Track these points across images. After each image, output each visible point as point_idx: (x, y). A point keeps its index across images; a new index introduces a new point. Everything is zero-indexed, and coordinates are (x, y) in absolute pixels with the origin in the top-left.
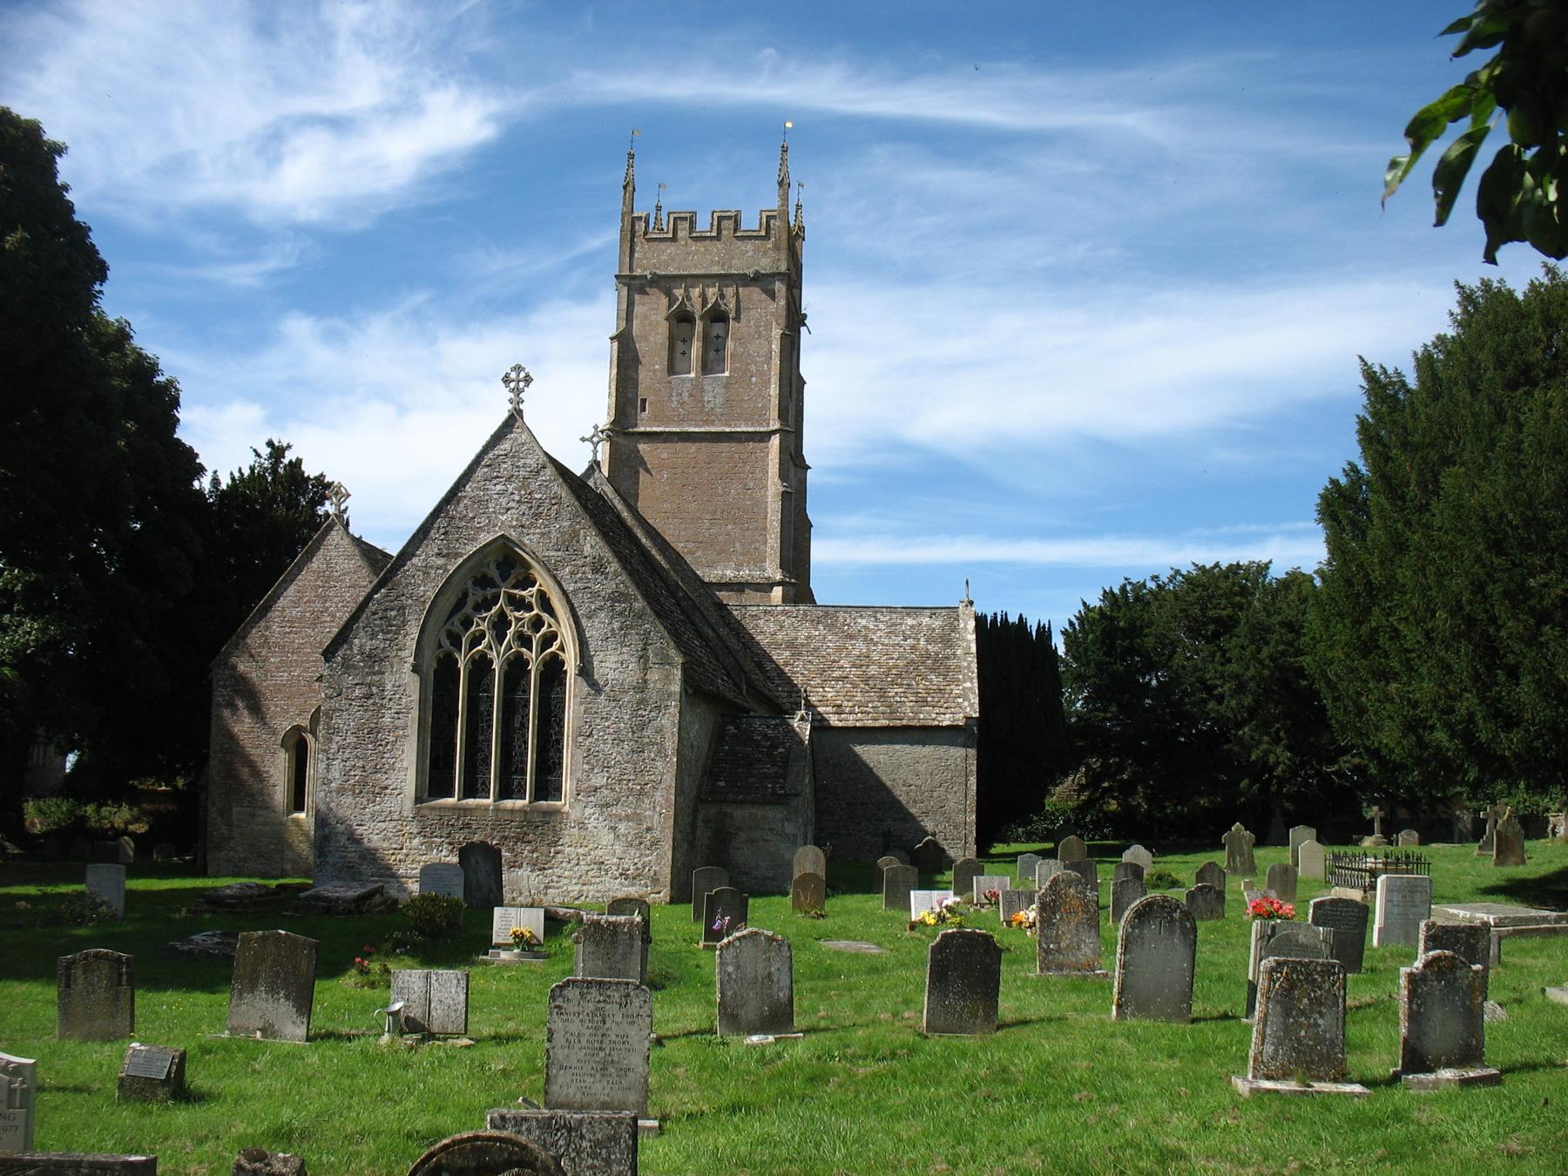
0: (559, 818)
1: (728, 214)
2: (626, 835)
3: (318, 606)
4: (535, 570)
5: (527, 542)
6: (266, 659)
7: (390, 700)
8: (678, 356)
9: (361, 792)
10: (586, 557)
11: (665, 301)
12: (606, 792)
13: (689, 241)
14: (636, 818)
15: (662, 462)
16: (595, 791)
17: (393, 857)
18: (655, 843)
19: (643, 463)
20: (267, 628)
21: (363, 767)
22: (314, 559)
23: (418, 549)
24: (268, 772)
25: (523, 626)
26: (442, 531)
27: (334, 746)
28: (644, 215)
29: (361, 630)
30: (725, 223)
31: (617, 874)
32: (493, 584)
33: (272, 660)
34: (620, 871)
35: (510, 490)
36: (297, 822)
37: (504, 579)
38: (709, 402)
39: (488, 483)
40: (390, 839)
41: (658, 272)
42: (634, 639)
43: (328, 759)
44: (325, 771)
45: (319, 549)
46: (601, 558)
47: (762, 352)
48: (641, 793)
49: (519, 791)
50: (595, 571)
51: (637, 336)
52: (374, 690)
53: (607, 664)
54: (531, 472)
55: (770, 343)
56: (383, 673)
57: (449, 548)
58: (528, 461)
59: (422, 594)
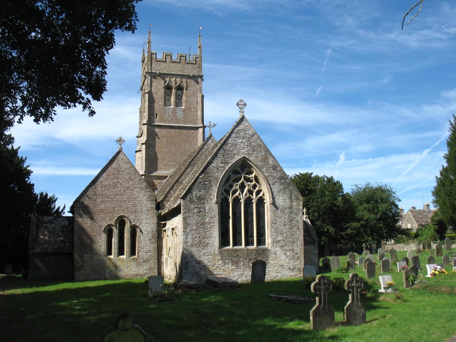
0: (268, 251)
1: (183, 55)
2: (289, 256)
3: (115, 181)
4: (254, 168)
5: (251, 159)
6: (96, 200)
7: (208, 213)
8: (166, 100)
9: (199, 246)
10: (270, 165)
11: (163, 82)
12: (282, 242)
13: (170, 63)
14: (292, 250)
15: (164, 135)
16: (279, 242)
17: (212, 268)
18: (298, 258)
19: (157, 135)
20: (96, 188)
21: (200, 237)
22: (113, 164)
23: (214, 160)
24: (98, 241)
25: (250, 187)
26: (222, 154)
27: (188, 230)
28: (155, 52)
29: (196, 189)
30: (168, 57)
31: (287, 269)
32: (239, 173)
33: (98, 200)
34: (288, 268)
35: (244, 142)
36: (110, 259)
37: (242, 172)
38: (178, 116)
39: (236, 139)
40: (211, 262)
41: (161, 72)
42: (287, 192)
43: (186, 234)
44: (185, 239)
45: (115, 160)
46: (275, 165)
47: (195, 101)
48: (293, 242)
49: (252, 243)
50: (274, 169)
51: (154, 93)
52: (202, 210)
53: (280, 200)
54: (250, 136)
55: (197, 98)
56: (205, 204)
57: (225, 160)
58: (249, 132)
59: (217, 176)
